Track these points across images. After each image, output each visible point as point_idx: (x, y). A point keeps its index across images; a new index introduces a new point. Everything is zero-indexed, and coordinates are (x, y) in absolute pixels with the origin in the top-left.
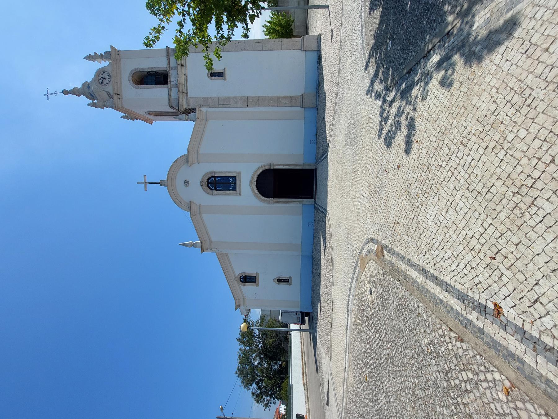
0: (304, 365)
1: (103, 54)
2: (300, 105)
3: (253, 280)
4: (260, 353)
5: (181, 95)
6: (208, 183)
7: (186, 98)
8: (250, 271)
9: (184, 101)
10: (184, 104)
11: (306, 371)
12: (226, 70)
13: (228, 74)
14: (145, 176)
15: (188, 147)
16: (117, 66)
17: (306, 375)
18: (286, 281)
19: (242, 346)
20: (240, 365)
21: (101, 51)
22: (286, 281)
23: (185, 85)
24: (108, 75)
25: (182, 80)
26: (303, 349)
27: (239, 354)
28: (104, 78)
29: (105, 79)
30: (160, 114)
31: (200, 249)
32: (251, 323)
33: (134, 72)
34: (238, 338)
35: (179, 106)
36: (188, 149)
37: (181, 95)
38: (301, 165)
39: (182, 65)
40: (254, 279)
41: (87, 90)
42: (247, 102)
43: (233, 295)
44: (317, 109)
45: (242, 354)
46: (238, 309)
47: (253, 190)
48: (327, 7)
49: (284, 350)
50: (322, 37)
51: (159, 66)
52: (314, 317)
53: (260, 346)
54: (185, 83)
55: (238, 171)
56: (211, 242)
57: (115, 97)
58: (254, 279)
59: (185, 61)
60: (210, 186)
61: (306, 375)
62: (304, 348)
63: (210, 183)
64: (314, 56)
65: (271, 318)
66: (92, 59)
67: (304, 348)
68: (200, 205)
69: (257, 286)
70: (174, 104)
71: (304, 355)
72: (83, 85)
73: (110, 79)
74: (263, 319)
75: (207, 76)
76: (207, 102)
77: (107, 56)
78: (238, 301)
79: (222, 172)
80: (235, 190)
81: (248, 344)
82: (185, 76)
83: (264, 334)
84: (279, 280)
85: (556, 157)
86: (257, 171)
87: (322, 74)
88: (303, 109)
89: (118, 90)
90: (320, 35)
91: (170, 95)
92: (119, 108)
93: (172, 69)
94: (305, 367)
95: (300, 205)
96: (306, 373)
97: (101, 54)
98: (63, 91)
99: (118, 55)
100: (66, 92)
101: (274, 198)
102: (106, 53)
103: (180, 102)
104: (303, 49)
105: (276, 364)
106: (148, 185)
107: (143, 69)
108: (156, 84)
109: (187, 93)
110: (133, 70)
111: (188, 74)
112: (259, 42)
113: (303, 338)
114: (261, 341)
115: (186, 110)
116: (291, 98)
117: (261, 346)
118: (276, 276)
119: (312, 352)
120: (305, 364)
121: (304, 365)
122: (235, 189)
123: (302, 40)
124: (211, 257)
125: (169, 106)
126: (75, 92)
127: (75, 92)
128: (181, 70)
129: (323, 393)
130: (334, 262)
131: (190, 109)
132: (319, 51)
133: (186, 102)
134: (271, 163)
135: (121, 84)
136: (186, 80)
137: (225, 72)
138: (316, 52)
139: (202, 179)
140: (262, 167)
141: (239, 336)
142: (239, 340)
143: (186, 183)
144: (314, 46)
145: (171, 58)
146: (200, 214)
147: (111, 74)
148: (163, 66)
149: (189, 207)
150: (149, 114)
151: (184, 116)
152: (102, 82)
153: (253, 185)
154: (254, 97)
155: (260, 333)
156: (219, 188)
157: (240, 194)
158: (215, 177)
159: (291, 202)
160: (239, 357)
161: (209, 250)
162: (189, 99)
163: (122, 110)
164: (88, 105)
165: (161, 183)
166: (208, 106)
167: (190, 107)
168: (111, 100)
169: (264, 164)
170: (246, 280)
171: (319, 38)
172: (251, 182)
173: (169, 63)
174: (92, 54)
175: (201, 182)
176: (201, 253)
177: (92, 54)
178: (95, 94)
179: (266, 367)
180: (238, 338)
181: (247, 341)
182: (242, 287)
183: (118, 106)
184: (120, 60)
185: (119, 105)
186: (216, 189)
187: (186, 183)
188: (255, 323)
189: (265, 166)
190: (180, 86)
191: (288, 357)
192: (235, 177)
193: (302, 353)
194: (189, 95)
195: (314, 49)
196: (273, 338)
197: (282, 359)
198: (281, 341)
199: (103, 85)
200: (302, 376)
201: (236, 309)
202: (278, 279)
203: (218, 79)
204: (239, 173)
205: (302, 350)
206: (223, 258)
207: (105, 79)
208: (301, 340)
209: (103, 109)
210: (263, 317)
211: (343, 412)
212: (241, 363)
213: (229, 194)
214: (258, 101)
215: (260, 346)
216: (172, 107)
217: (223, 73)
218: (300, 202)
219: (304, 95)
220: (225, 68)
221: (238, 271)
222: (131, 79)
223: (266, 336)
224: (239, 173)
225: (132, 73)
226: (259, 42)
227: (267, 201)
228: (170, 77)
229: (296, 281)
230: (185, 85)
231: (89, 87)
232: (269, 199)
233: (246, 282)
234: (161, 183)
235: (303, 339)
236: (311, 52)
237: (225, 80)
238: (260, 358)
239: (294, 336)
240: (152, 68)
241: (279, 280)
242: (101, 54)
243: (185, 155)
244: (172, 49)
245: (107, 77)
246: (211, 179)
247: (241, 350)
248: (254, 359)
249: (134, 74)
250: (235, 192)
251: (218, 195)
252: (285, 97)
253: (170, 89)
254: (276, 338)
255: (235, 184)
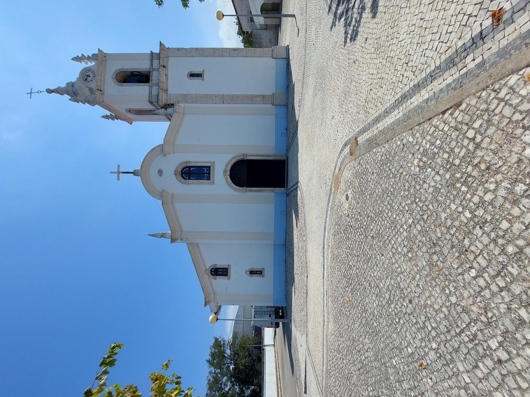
0: (279, 380)
1: (91, 56)
2: (272, 102)
3: (225, 273)
4: (231, 376)
5: (161, 92)
6: (182, 173)
7: (165, 94)
8: (221, 263)
9: (164, 97)
10: (164, 99)
11: (281, 387)
12: (204, 72)
13: (206, 75)
14: (119, 166)
15: (165, 138)
16: (102, 66)
17: (281, 391)
18: (259, 273)
19: (212, 369)
20: (209, 392)
21: (89, 53)
22: (259, 273)
23: (166, 84)
24: (93, 73)
25: (163, 78)
26: (277, 363)
27: (208, 379)
28: (89, 76)
29: (90, 76)
30: (140, 113)
31: (170, 240)
32: (222, 342)
33: (118, 71)
34: (208, 360)
35: (159, 101)
36: (164, 140)
37: (161, 92)
38: (273, 156)
39: (164, 67)
40: (225, 272)
41: (71, 88)
42: (223, 99)
43: (203, 289)
44: (287, 106)
45: (211, 379)
46: (208, 306)
47: (227, 180)
48: (294, 16)
49: (258, 371)
50: (290, 47)
51: (143, 67)
52: (288, 313)
53: (231, 368)
54: (166, 81)
55: (212, 160)
56: (181, 231)
57: (98, 93)
58: (225, 272)
59: (167, 63)
60: (184, 176)
61: (281, 391)
62: (278, 362)
63: (184, 173)
64: (284, 62)
65: (243, 336)
66: (79, 60)
67: (278, 362)
68: (173, 194)
69: (229, 279)
70: (154, 100)
71: (279, 369)
72: (67, 84)
73: (94, 76)
74: (235, 337)
75: (187, 77)
76: (185, 98)
77: (94, 57)
78: (208, 297)
79: (196, 162)
80: (209, 179)
81: (218, 365)
82: (166, 76)
83: (235, 354)
84: (252, 272)
85: (483, 31)
86: (230, 161)
87: (291, 72)
88: (274, 106)
89: (101, 86)
90: (288, 46)
91: (150, 92)
92: (100, 103)
93: (154, 70)
94: (280, 382)
95: (273, 194)
96: (281, 388)
97: (88, 56)
98: (47, 90)
99: (105, 57)
100: (49, 91)
101: (246, 187)
102: (94, 55)
103: (160, 98)
104: (273, 57)
105: (248, 388)
106: (121, 174)
107: (127, 69)
108: (138, 83)
109: (167, 90)
110: (117, 70)
111: (169, 75)
112: (235, 50)
113: (277, 351)
114: (232, 362)
115: (165, 106)
116: (263, 97)
117: (233, 368)
118: (249, 267)
119: (286, 356)
120: (280, 379)
121: (279, 380)
122: (208, 178)
123: (272, 49)
124: (181, 247)
125: (149, 102)
126: (59, 91)
127: (59, 91)
128: (163, 71)
129: (300, 382)
130: (308, 226)
131: (169, 105)
132: (288, 59)
133: (165, 98)
134: (244, 154)
135: (105, 81)
136: (167, 79)
137: (203, 73)
138: (285, 59)
139: (176, 168)
140: (235, 157)
141: (209, 358)
142: (208, 361)
143: (160, 172)
144: (284, 55)
145: (154, 61)
146: (172, 203)
147: (96, 73)
148: (146, 68)
149: (161, 195)
150: (130, 111)
151: (163, 111)
152: (86, 79)
153: (227, 174)
154: (230, 95)
155: (231, 354)
156: (193, 178)
157: (213, 183)
158: (190, 167)
159: (264, 190)
160: (208, 382)
161: (179, 240)
162: (169, 96)
163: (103, 105)
164: (72, 59)
165: (135, 173)
166: (187, 102)
167: (169, 103)
168: (93, 95)
169: (237, 154)
170: (217, 273)
171: (287, 49)
172: (225, 171)
173: (152, 65)
174: (80, 56)
175: (175, 171)
176: (171, 243)
177: (80, 56)
178: (78, 91)
179: (237, 393)
180: (208, 360)
181: (217, 362)
182: (212, 280)
183: (99, 101)
184: (106, 61)
185: (100, 100)
186: (190, 179)
187: (160, 172)
188: (227, 343)
189: (240, 156)
190: (161, 84)
191: (261, 378)
192: (209, 167)
193: (276, 368)
194: (169, 92)
195: (284, 57)
196: (246, 358)
197: (255, 381)
198: (254, 361)
199: (87, 82)
200: (276, 394)
201: (205, 305)
202: (250, 272)
203: (197, 79)
204: (213, 163)
205: (276, 365)
206: (193, 248)
207: (90, 76)
208: (275, 354)
209: (84, 104)
210: (235, 335)
211: (324, 378)
212: (210, 388)
213: (202, 183)
214: (234, 99)
215: (231, 368)
216: (151, 103)
217: (201, 74)
218: (272, 191)
219: (275, 94)
220: (203, 70)
221: (210, 262)
222: (115, 77)
223: (238, 356)
224: (213, 163)
225: (116, 73)
226: (235, 50)
227: (240, 189)
228: (152, 77)
229: (269, 272)
230: (166, 84)
231: (73, 86)
232: (242, 188)
233: (217, 275)
234: (135, 173)
235: (277, 353)
236: (281, 59)
237: (203, 80)
238: (231, 382)
239: (268, 351)
240: (136, 69)
241: (252, 272)
242: (88, 56)
243: (161, 145)
244: (156, 53)
245: (91, 75)
246: (186, 169)
247: (210, 373)
248: (224, 385)
249: (117, 73)
250: (208, 181)
251: (190, 184)
252: (258, 96)
253: (151, 87)
254: (249, 358)
255: (209, 174)
